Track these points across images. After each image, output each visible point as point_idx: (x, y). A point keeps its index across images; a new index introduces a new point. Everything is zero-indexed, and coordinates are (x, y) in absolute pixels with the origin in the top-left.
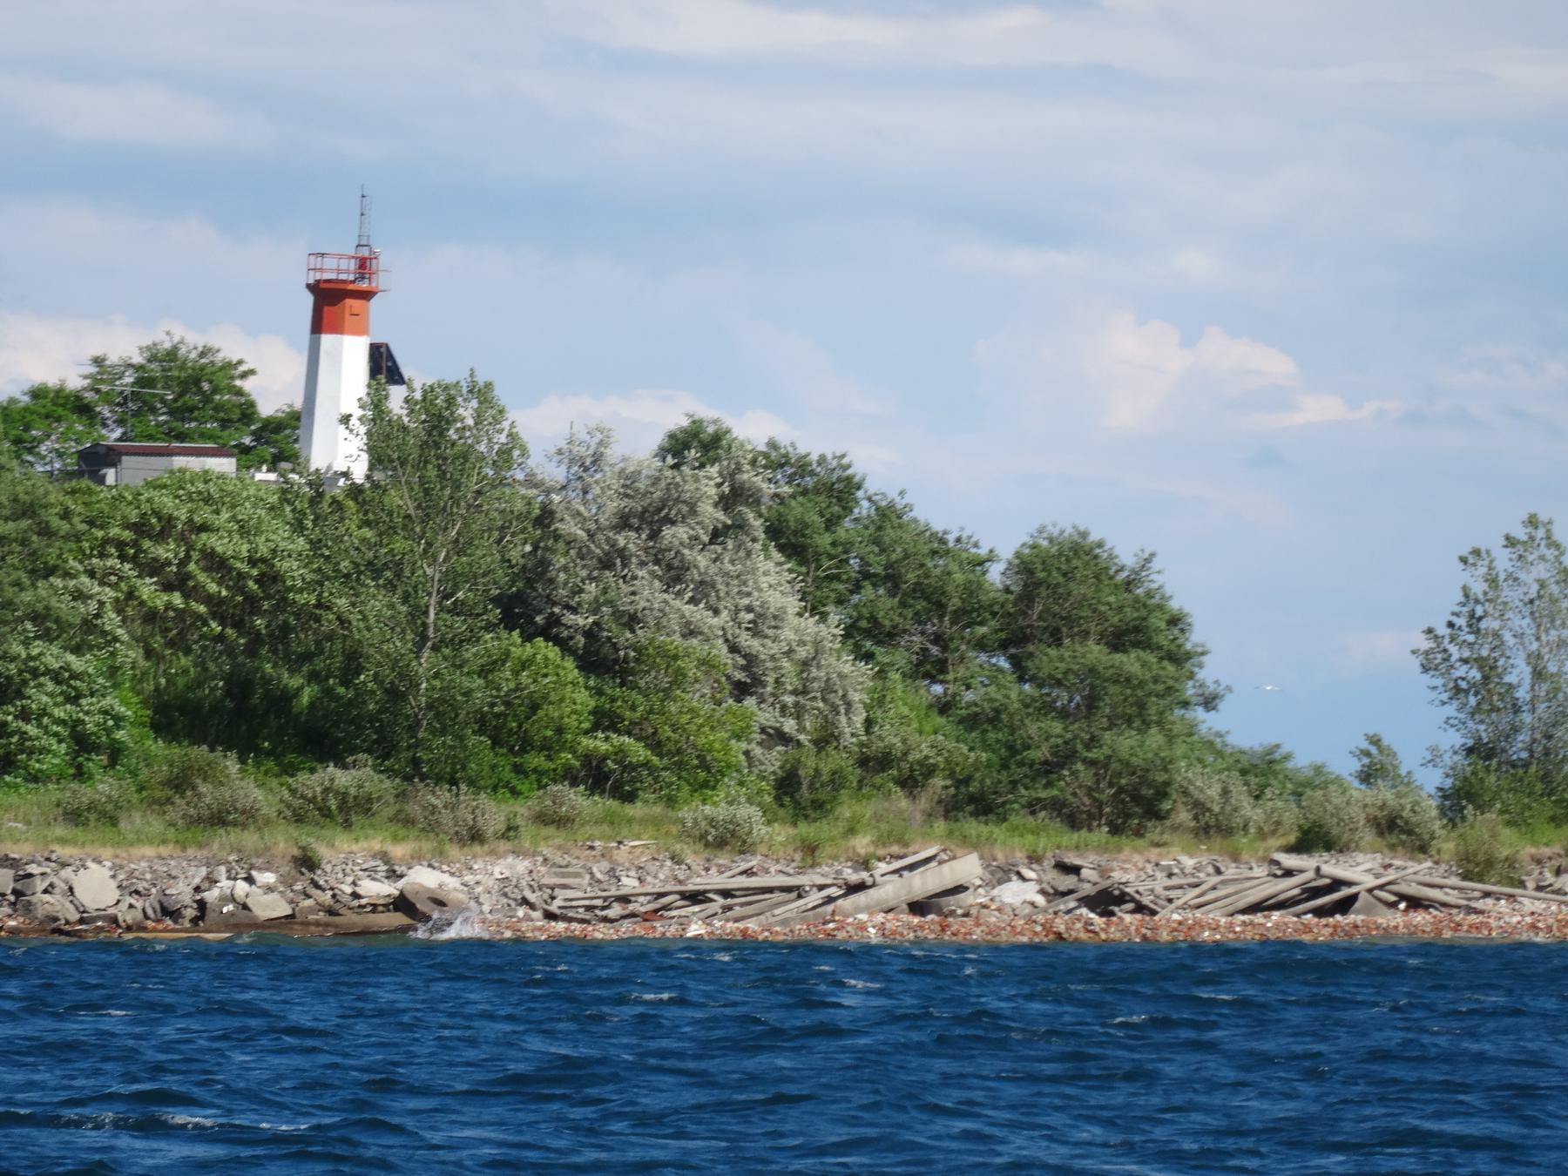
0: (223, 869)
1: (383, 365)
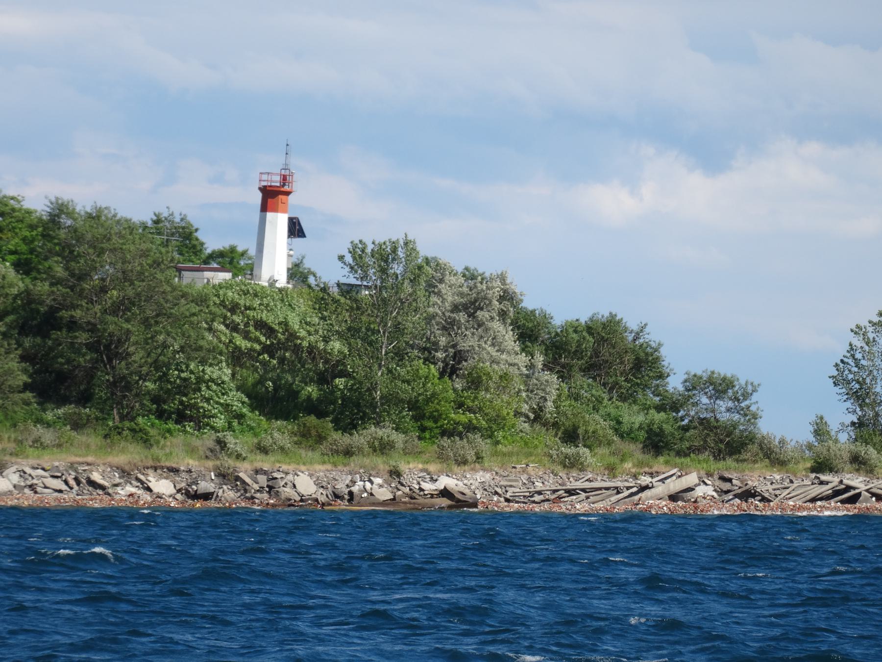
0: (358, 476)
1: (295, 229)
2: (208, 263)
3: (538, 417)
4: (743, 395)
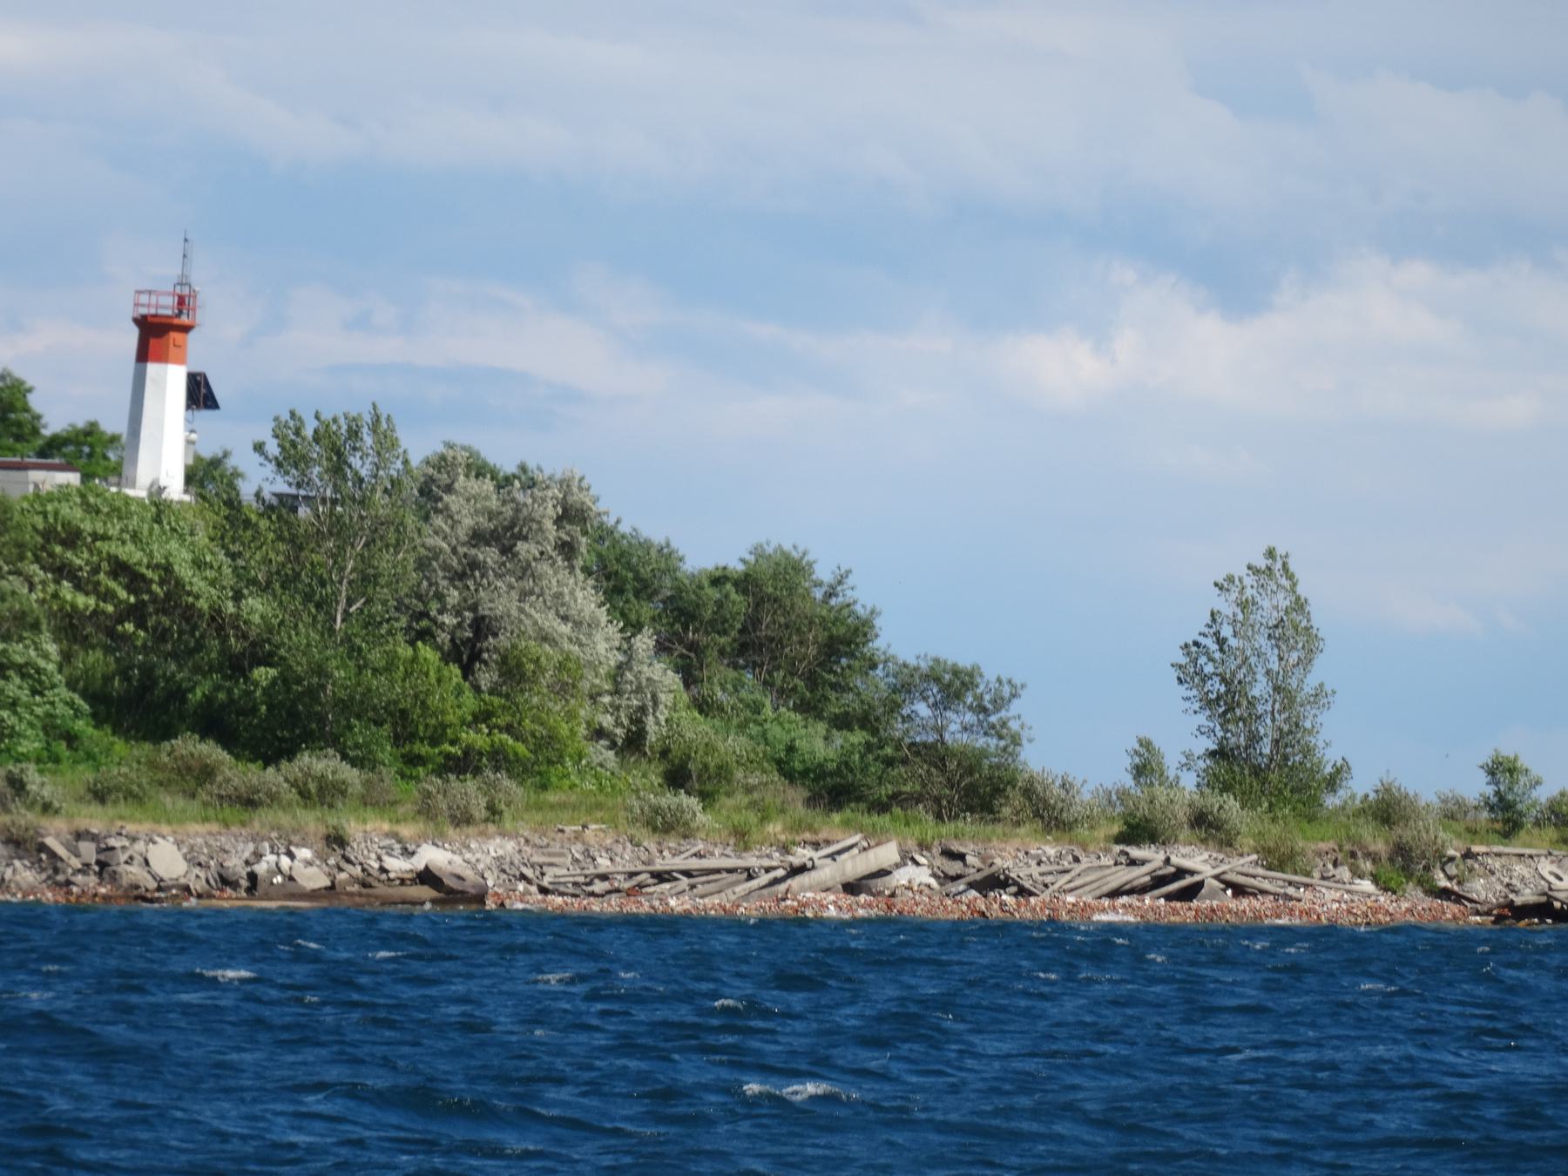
0: (266, 845)
1: (200, 394)
2: (51, 456)
3: (634, 742)
4: (994, 701)
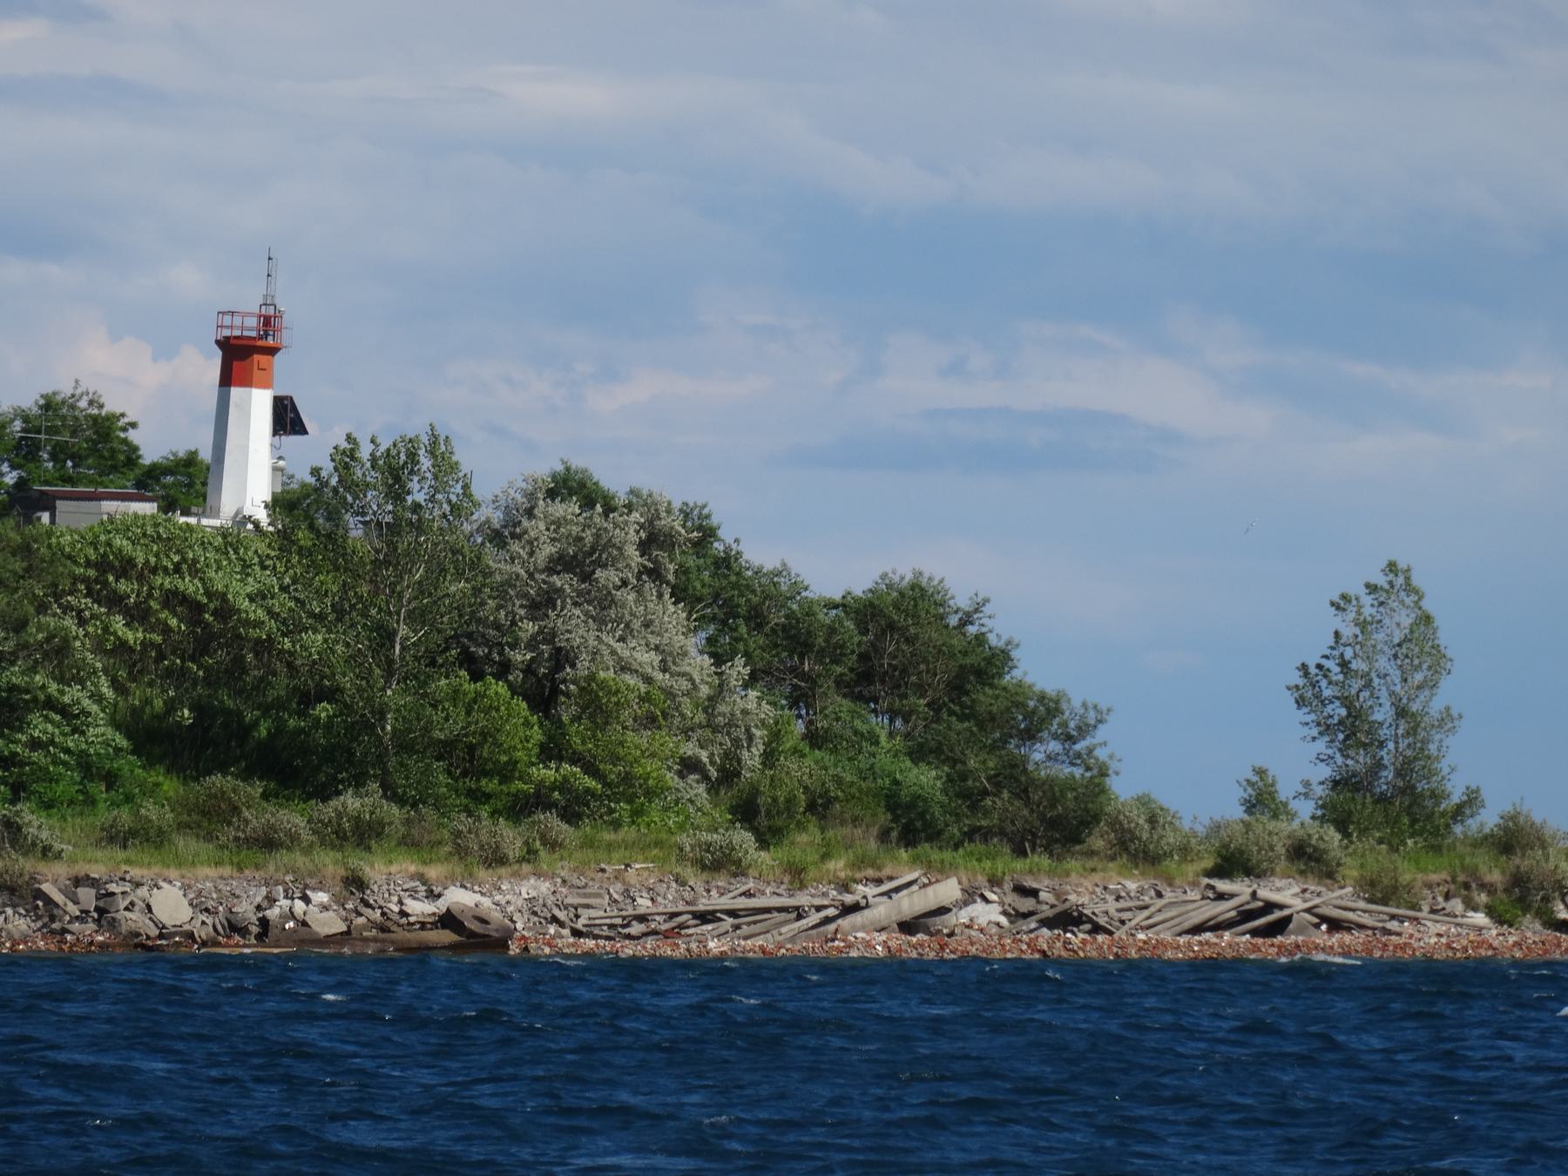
0: (280, 888)
1: (287, 419)
4: (1079, 728)
